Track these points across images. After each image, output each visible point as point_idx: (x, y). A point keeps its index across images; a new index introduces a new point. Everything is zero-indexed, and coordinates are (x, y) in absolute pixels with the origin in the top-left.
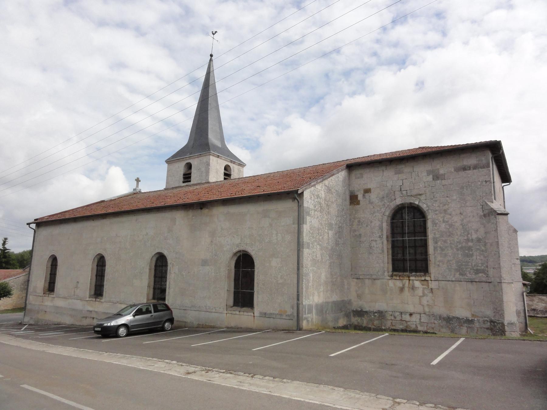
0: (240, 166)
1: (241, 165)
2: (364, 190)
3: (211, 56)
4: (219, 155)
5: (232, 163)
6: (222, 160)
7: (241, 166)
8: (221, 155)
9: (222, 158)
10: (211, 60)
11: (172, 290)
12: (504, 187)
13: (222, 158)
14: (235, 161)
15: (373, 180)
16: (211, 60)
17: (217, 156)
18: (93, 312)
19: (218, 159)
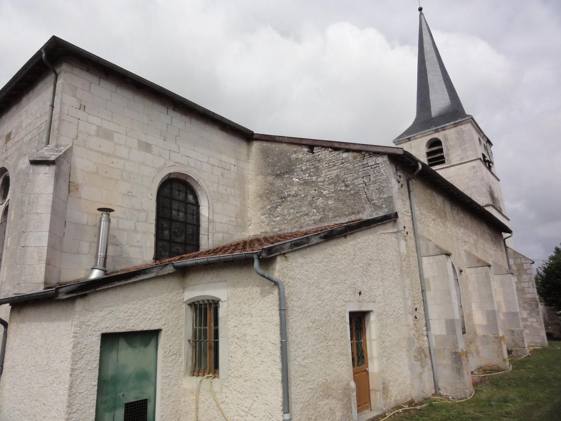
0: (458, 125)
1: (464, 122)
2: (445, 163)
3: (420, 9)
4: (408, 137)
5: (439, 131)
6: (418, 140)
7: (461, 125)
8: (412, 136)
9: (416, 137)
10: (421, 14)
11: (374, 344)
12: (506, 240)
13: (416, 137)
14: (442, 126)
15: (314, 178)
16: (421, 14)
17: (407, 140)
18: (110, 372)
19: (411, 142)
